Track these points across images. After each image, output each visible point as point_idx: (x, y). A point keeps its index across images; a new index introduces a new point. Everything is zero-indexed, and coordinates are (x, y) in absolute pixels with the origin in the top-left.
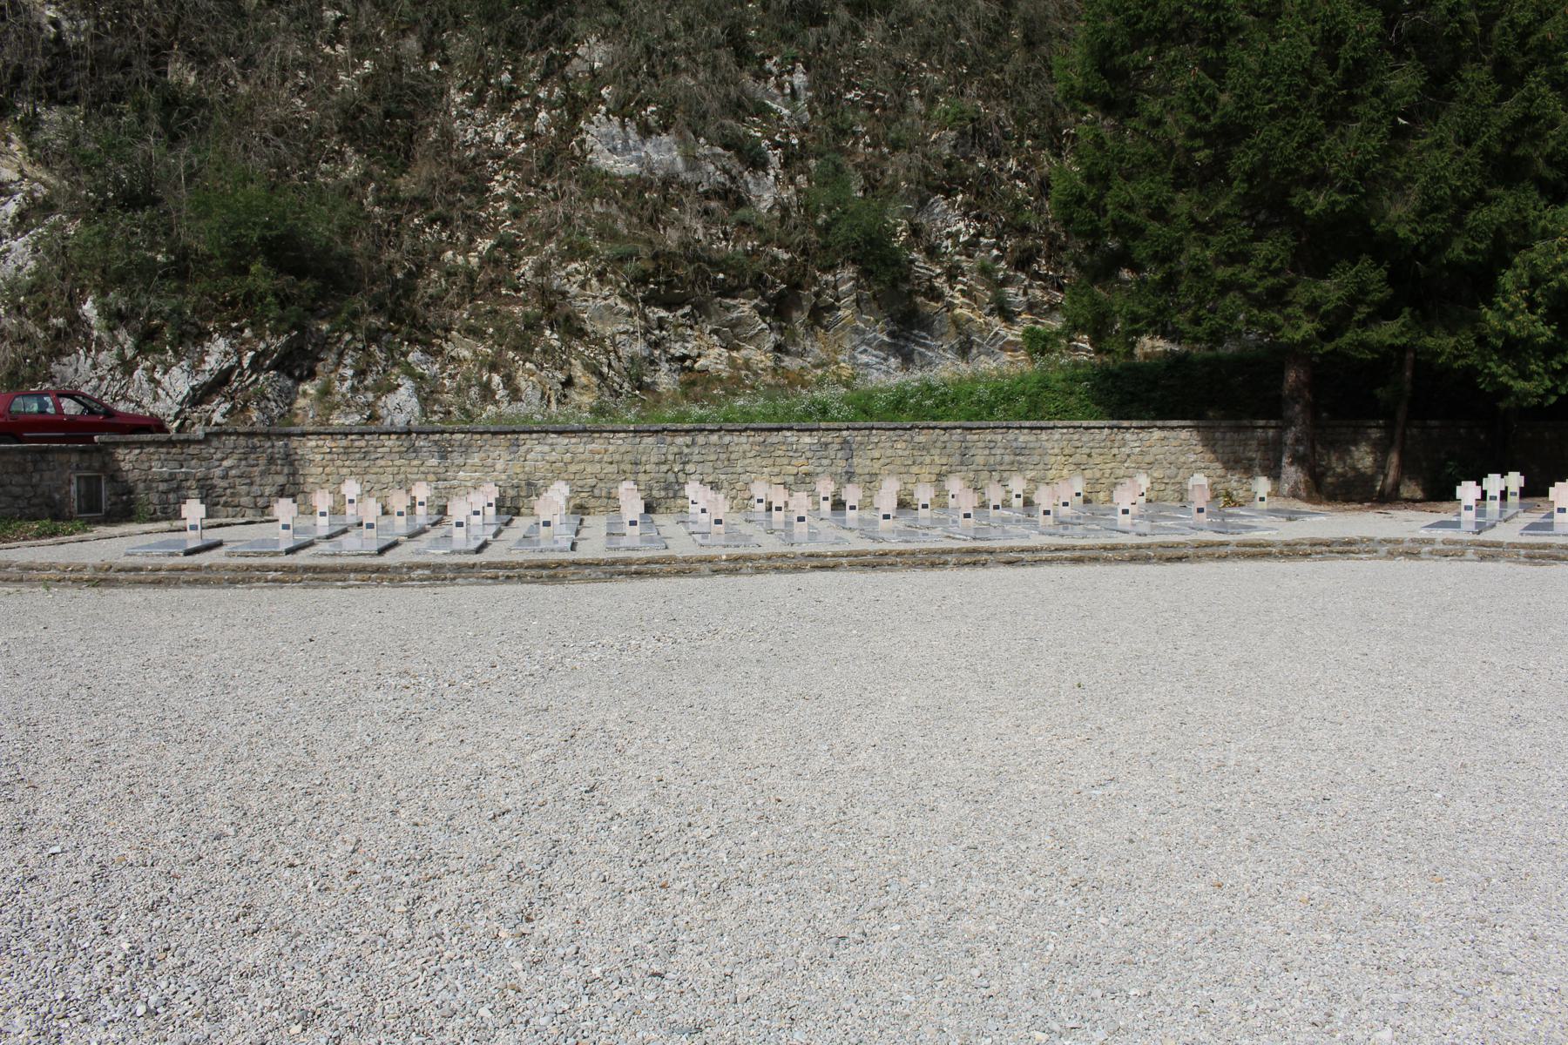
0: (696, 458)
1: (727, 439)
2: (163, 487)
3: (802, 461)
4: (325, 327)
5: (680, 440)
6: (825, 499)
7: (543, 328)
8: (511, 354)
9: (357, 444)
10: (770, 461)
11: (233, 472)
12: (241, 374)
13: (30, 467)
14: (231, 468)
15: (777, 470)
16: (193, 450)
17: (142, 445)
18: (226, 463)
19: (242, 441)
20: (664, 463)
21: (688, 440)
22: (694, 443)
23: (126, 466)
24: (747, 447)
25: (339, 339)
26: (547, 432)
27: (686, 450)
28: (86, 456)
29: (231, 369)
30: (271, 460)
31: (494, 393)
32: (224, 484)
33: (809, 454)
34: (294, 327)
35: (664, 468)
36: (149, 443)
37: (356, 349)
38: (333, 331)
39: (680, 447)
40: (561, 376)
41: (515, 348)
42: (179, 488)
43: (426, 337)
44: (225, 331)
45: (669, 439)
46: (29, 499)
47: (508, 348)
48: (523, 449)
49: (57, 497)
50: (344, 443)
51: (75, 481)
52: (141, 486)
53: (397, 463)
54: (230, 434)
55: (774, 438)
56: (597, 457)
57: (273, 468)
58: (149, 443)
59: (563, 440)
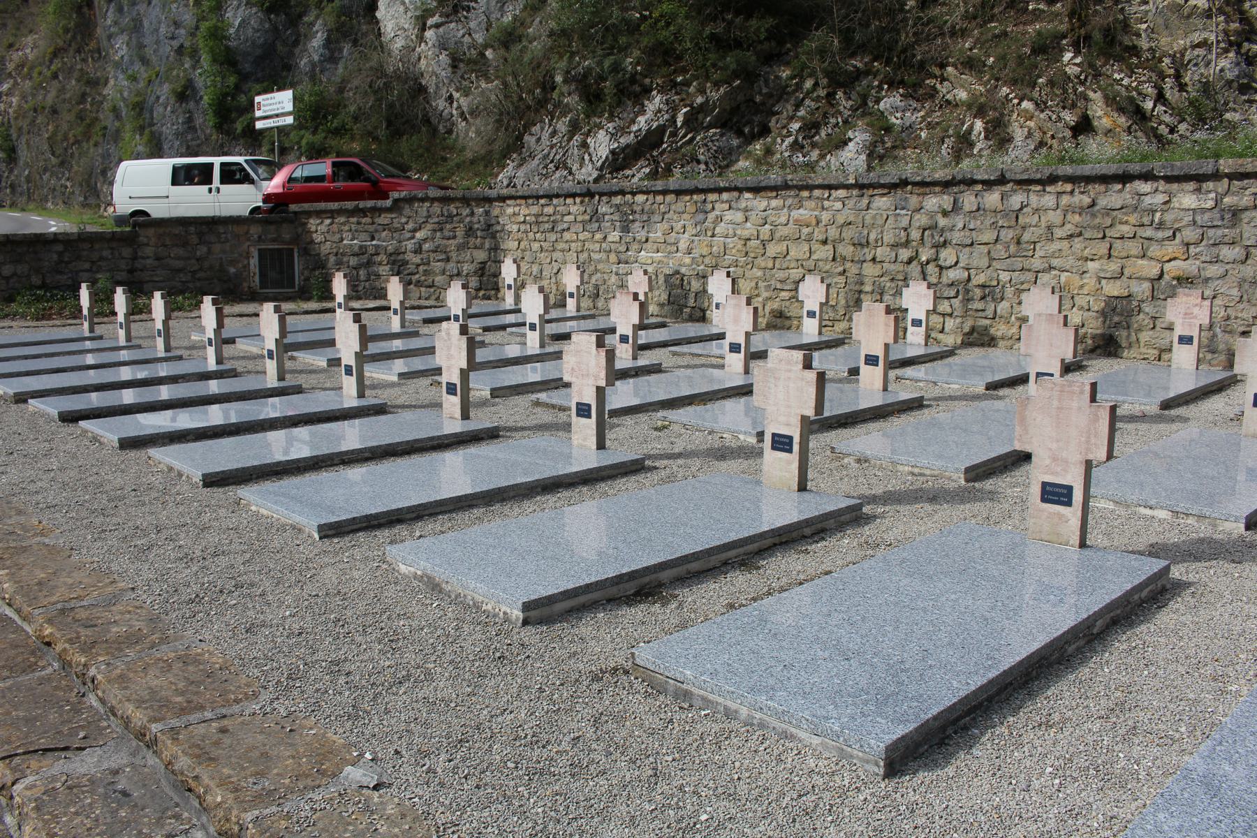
0: (956, 237)
1: (1016, 200)
2: (353, 261)
3: (1172, 248)
4: (785, 73)
5: (933, 202)
6: (1186, 340)
7: (1062, 51)
8: (1005, 90)
9: (546, 210)
10: (1102, 248)
11: (426, 246)
12: (674, 134)
13: (194, 239)
14: (425, 240)
15: (1114, 267)
16: (384, 219)
17: (332, 214)
18: (419, 235)
19: (436, 208)
20: (907, 244)
21: (946, 201)
22: (956, 208)
23: (318, 238)
24: (1055, 217)
25: (799, 87)
26: (740, 190)
27: (942, 222)
28: (272, 228)
29: (661, 130)
30: (470, 231)
31: (972, 145)
32: (417, 260)
33: (1190, 234)
34: (736, 75)
35: (905, 254)
36: (340, 212)
37: (818, 99)
38: (793, 77)
39: (932, 215)
40: (1070, 117)
41: (1013, 82)
42: (369, 263)
43: (914, 78)
44: (671, 86)
45: (914, 200)
46: (194, 272)
47: (1005, 84)
48: (711, 216)
49: (232, 270)
50: (535, 209)
51: (256, 254)
52: (332, 259)
53: (581, 237)
54: (423, 200)
55: (1114, 197)
56: (805, 231)
57: (472, 241)
58: (340, 212)
59: (759, 203)
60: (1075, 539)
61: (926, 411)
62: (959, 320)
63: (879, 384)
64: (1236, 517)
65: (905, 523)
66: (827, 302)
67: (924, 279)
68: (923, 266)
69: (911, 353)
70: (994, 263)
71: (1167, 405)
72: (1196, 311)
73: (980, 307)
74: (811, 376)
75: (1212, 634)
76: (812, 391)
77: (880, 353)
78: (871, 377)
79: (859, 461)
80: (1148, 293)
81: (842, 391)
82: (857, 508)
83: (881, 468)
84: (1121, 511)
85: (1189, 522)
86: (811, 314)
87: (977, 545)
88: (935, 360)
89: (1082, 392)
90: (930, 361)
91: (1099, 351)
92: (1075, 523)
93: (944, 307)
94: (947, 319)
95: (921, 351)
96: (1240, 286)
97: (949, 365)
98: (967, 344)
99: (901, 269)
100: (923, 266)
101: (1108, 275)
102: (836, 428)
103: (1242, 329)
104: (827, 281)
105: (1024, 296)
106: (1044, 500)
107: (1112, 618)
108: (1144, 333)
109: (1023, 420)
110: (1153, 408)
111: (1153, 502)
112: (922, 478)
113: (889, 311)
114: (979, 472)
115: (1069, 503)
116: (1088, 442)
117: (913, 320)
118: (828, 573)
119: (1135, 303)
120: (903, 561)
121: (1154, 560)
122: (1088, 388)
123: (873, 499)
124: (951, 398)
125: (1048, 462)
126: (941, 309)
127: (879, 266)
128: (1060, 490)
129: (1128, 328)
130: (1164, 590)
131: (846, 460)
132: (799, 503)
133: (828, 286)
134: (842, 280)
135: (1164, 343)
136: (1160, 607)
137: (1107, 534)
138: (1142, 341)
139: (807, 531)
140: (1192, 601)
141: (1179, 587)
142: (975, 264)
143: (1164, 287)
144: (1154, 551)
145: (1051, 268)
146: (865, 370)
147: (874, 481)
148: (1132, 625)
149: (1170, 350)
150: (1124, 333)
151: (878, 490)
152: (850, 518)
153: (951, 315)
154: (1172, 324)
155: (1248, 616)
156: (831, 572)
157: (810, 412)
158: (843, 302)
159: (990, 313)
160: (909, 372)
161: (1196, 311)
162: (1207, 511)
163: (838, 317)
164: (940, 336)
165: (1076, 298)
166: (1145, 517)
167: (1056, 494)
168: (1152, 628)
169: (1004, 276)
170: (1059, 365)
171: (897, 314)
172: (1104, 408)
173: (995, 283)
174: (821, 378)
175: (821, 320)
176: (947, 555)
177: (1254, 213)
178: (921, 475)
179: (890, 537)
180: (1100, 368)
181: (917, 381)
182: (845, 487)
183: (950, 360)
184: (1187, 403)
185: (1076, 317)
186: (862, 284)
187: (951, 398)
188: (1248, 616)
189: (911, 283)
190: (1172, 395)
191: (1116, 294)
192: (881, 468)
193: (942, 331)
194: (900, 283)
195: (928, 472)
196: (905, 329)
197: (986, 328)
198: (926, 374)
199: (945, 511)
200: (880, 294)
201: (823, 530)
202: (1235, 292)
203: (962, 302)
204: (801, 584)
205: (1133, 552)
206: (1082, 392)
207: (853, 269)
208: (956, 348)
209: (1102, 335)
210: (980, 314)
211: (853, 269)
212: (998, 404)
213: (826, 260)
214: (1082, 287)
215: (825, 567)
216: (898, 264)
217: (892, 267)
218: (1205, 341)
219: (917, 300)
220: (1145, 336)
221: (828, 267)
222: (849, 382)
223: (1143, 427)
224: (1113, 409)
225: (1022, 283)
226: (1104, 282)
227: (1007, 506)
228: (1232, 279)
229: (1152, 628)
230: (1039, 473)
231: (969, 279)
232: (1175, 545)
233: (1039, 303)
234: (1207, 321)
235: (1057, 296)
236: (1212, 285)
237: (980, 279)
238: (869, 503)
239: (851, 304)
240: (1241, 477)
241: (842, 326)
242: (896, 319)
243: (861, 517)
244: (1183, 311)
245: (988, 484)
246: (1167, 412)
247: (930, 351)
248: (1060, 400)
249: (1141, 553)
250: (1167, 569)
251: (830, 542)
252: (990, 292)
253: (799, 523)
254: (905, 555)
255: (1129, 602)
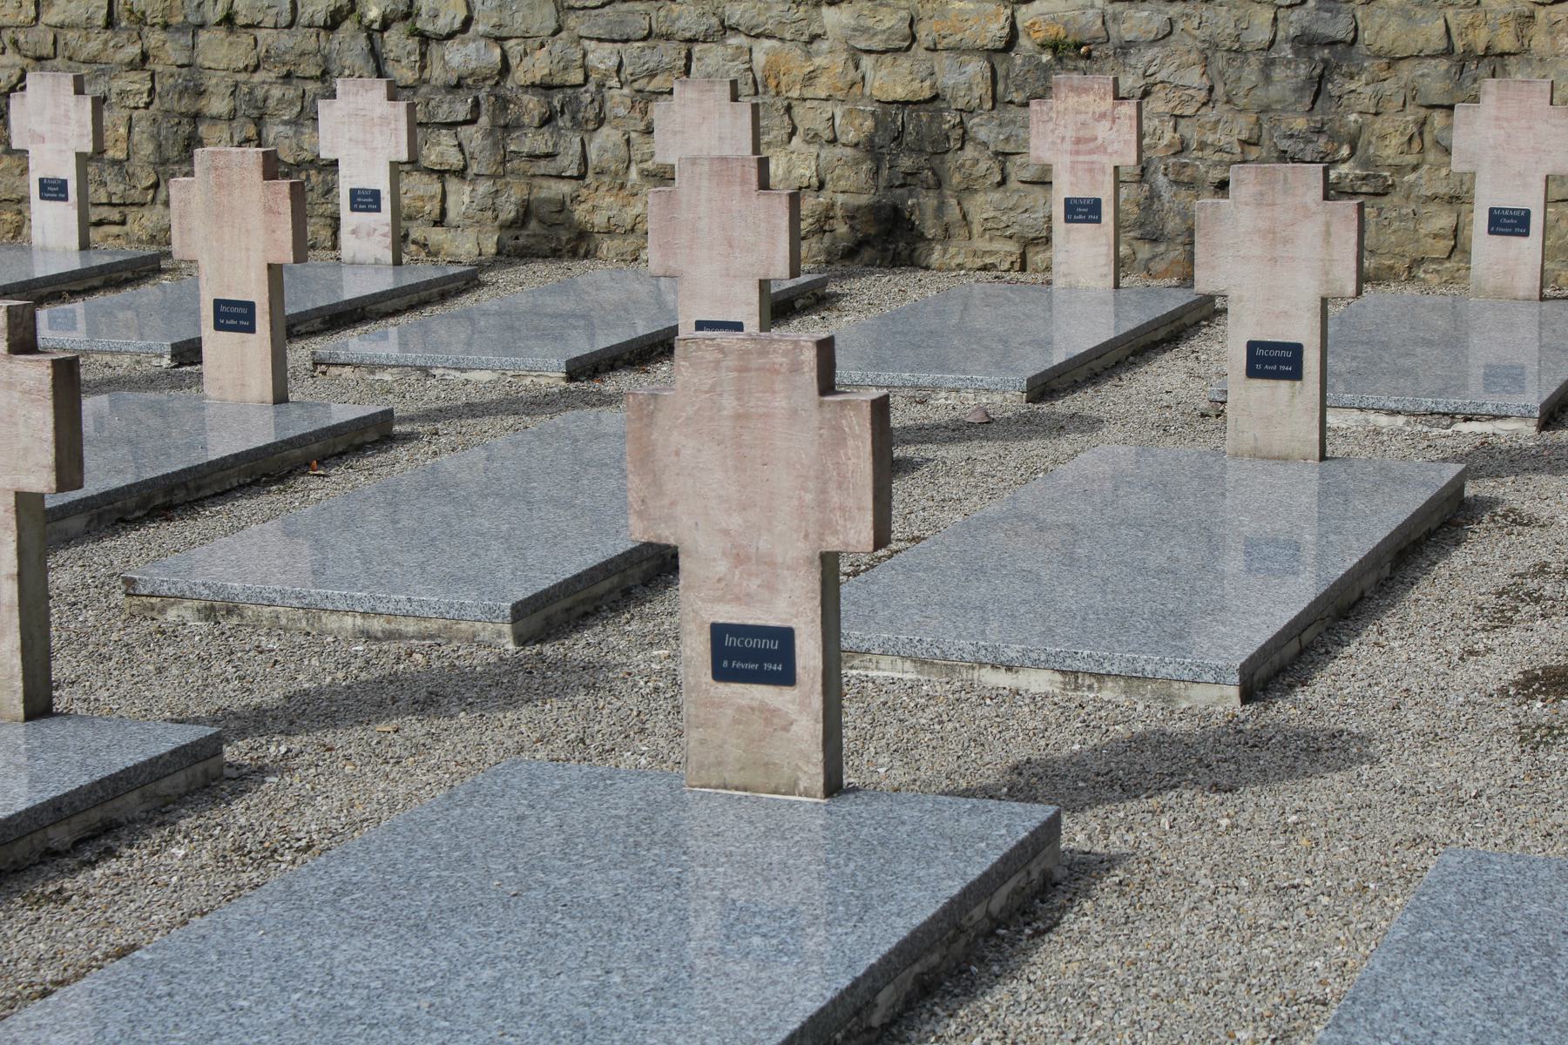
6: (1083, 211)
60: (813, 774)
61: (401, 452)
62: (484, 187)
63: (260, 384)
64: (1218, 671)
65: (349, 780)
66: (99, 150)
67: (380, 73)
68: (374, 33)
69: (355, 287)
70: (571, 21)
71: (1044, 388)
72: (1102, 130)
73: (542, 149)
74: (36, 373)
75: (1168, 986)
76: (42, 418)
77: (255, 290)
78: (238, 365)
79: (209, 613)
80: (981, 89)
81: (162, 412)
82: (207, 750)
83: (275, 627)
84: (936, 684)
85: (1106, 695)
86: (53, 190)
87: (550, 820)
88: (424, 303)
89: (795, 368)
90: (412, 308)
91: (867, 254)
92: (807, 728)
93: (441, 150)
94: (453, 184)
95: (383, 282)
96: (1206, 62)
97: (468, 316)
98: (511, 254)
99: (311, 44)
100: (374, 33)
101: (876, 44)
102: (139, 522)
103: (1216, 175)
104: (91, 90)
105: (658, 109)
106: (720, 674)
107: (918, 979)
108: (980, 198)
109: (646, 457)
110: (1010, 401)
111: (1012, 653)
112: (393, 647)
113: (272, 168)
114: (554, 614)
115: (787, 677)
116: (822, 504)
117: (354, 193)
118: (122, 953)
119: (951, 118)
120: (342, 891)
121: (1017, 807)
122: (810, 356)
123: (258, 721)
124: (474, 410)
125: (722, 567)
126: (431, 156)
127: (246, 39)
128: (762, 644)
129: (939, 185)
130: (1048, 885)
131: (172, 615)
132: (31, 756)
133: (99, 103)
134: (137, 83)
135: (1029, 223)
136: (1039, 933)
137: (902, 751)
138: (976, 218)
139: (60, 836)
140: (1119, 904)
141: (1085, 871)
142: (518, 24)
143: (1024, 67)
144: (1023, 783)
145: (726, 29)
146: (218, 346)
147: (257, 666)
148: (971, 991)
149: (1048, 240)
150: (929, 201)
151: (271, 693)
152: (191, 780)
153: (461, 173)
154: (1047, 169)
155: (1254, 927)
156: (134, 947)
157: (41, 480)
158: (147, 149)
159: (568, 162)
160: (353, 342)
161: (1102, 130)
162: (1147, 662)
163: (136, 195)
164: (437, 236)
165: (798, 110)
166: (996, 695)
167: (750, 655)
168: (1024, 991)
169: (602, 57)
170: (755, 297)
171: (305, 182)
172: (856, 406)
173: (578, 77)
174: (68, 381)
175: (84, 206)
176: (467, 858)
177: (5, 21)
178: (391, 636)
179: (307, 824)
180: (871, 304)
181: (374, 367)
182: (168, 693)
183: (467, 301)
184: (1094, 378)
185: (794, 163)
186: (200, 93)
187: (474, 410)
188: (1254, 927)
189: (339, 84)
190: (1058, 358)
191: (900, 93)
192: (275, 627)
193: (440, 221)
194: (311, 87)
195: (410, 626)
196: (335, 222)
197: (562, 206)
198: (404, 345)
199: (462, 733)
200: (253, 119)
201: (109, 828)
202: (1194, 77)
203: (490, 133)
204: (45, 994)
205: (968, 793)
206: (795, 368)
207: (170, 52)
208: (481, 267)
209: (874, 209)
210: (543, 166)
211: (170, 52)
212: (610, 418)
213: (88, 26)
214: (810, 78)
215: (116, 937)
216: (299, 32)
217: (285, 40)
218: (1132, 212)
219: (361, 133)
220: (982, 206)
221: (94, 46)
222: (177, 383)
223: (985, 451)
224: (881, 408)
225: (652, 75)
226: (867, 62)
227: (632, 701)
228: (1186, 44)
229: (1024, 991)
230: (703, 602)
231: (505, 69)
232: (1076, 761)
233: (699, 126)
234: (1131, 158)
235: (745, 107)
236: (1140, 59)
237: (536, 66)
238: (242, 734)
239: (173, 153)
240: (1233, 563)
241: (142, 223)
242: (298, 193)
243: (219, 777)
244: (1070, 133)
245: (580, 646)
246: (1044, 408)
247: (409, 279)
248: (740, 394)
249: (988, 793)
250: (1052, 827)
251: (131, 861)
252: (565, 103)
253: (32, 814)
254: (346, 871)
255: (960, 930)
